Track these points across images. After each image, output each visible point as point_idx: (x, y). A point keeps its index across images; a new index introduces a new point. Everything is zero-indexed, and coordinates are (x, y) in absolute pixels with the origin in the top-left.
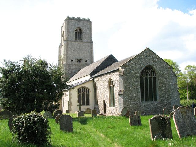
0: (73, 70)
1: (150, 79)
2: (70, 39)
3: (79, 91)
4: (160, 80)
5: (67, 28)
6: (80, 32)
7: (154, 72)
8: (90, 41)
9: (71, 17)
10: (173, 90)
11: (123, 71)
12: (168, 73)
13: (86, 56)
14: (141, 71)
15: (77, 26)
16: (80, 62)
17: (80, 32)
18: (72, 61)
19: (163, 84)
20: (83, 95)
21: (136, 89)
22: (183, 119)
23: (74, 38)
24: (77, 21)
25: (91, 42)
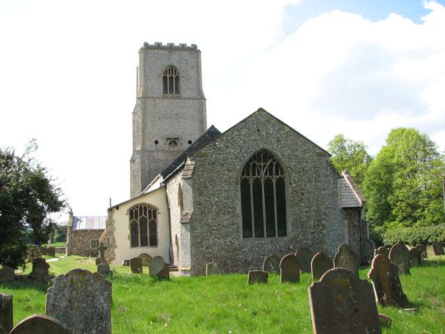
0: (160, 164)
1: (268, 183)
2: (150, 94)
3: (132, 213)
4: (294, 185)
5: (144, 69)
6: (174, 76)
7: (278, 165)
8: (199, 95)
9: (152, 43)
10: (329, 208)
11: (192, 167)
12: (315, 167)
13: (188, 131)
14: (242, 167)
15: (166, 63)
16: (176, 144)
17: (174, 76)
18: (156, 142)
19: (303, 194)
20: (143, 221)
21: (229, 207)
22: (70, 301)
23: (162, 90)
24: (166, 52)
25: (201, 98)
